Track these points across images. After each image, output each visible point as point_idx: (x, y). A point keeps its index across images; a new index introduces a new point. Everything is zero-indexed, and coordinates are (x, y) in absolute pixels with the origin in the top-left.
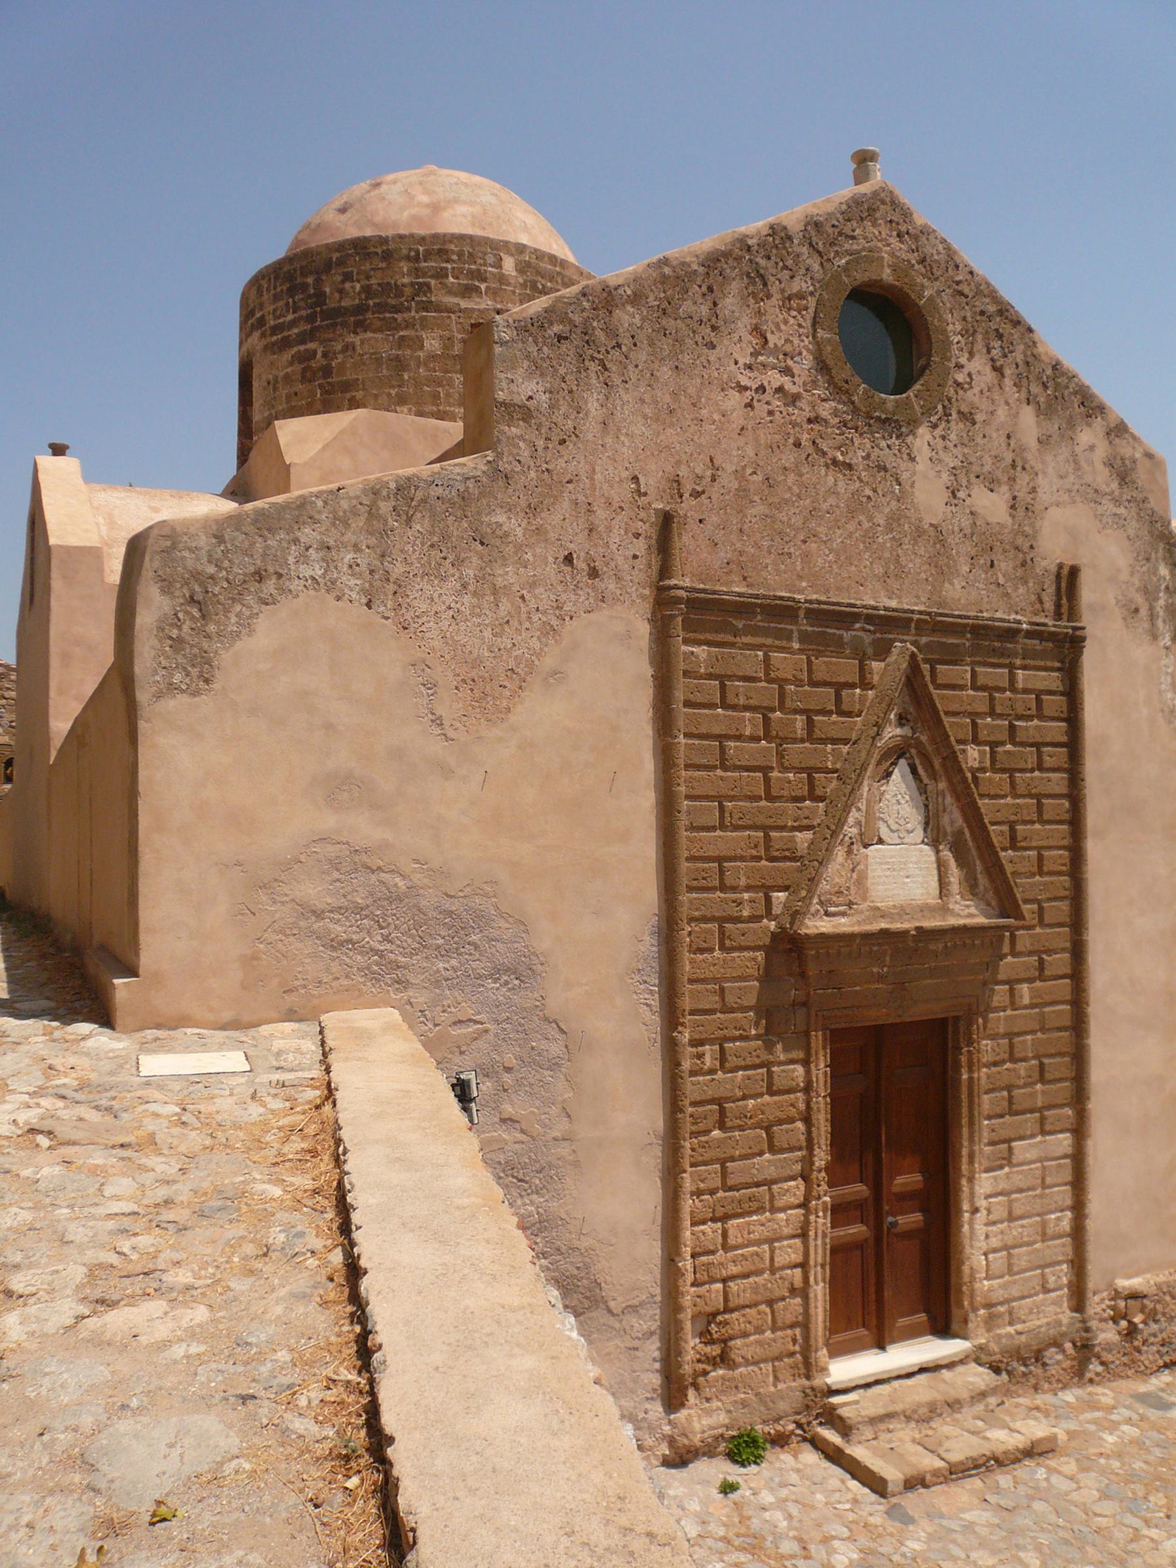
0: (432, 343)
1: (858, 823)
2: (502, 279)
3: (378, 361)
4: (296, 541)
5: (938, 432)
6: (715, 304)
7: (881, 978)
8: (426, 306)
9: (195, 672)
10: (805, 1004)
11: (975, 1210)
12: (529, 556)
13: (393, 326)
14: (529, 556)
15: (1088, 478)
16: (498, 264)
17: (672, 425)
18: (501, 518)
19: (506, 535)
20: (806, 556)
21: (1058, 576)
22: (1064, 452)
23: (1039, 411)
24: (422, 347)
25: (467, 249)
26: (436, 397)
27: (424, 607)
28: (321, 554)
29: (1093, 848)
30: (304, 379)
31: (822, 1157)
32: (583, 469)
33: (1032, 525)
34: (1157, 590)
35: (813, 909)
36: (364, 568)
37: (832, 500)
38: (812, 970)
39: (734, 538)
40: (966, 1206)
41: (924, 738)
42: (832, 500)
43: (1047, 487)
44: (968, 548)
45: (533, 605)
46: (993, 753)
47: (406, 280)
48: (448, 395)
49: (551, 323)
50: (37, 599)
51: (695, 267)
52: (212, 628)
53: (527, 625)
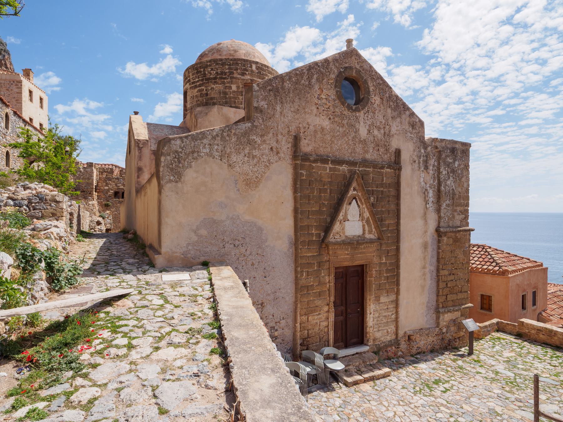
0: (234, 87)
1: (343, 215)
2: (252, 71)
4: (202, 143)
5: (365, 115)
6: (310, 81)
7: (348, 254)
9: (176, 176)
10: (328, 261)
11: (370, 314)
12: (262, 147)
14: (262, 147)
15: (404, 127)
16: (251, 67)
17: (298, 113)
18: (255, 138)
19: (256, 142)
20: (331, 147)
21: (395, 153)
22: (398, 120)
23: (392, 109)
24: (231, 89)
26: (235, 102)
27: (235, 160)
28: (209, 146)
29: (402, 221)
30: (201, 97)
32: (276, 125)
33: (389, 139)
34: (421, 156)
35: (331, 237)
36: (220, 150)
37: (338, 133)
38: (331, 253)
39: (313, 143)
40: (368, 312)
41: (360, 194)
42: (338, 133)
43: (394, 130)
44: (372, 145)
45: (262, 160)
46: (377, 198)
47: (227, 71)
48: (238, 102)
49: (268, 86)
50: (131, 153)
51: (304, 71)
52: (181, 165)
53: (261, 165)
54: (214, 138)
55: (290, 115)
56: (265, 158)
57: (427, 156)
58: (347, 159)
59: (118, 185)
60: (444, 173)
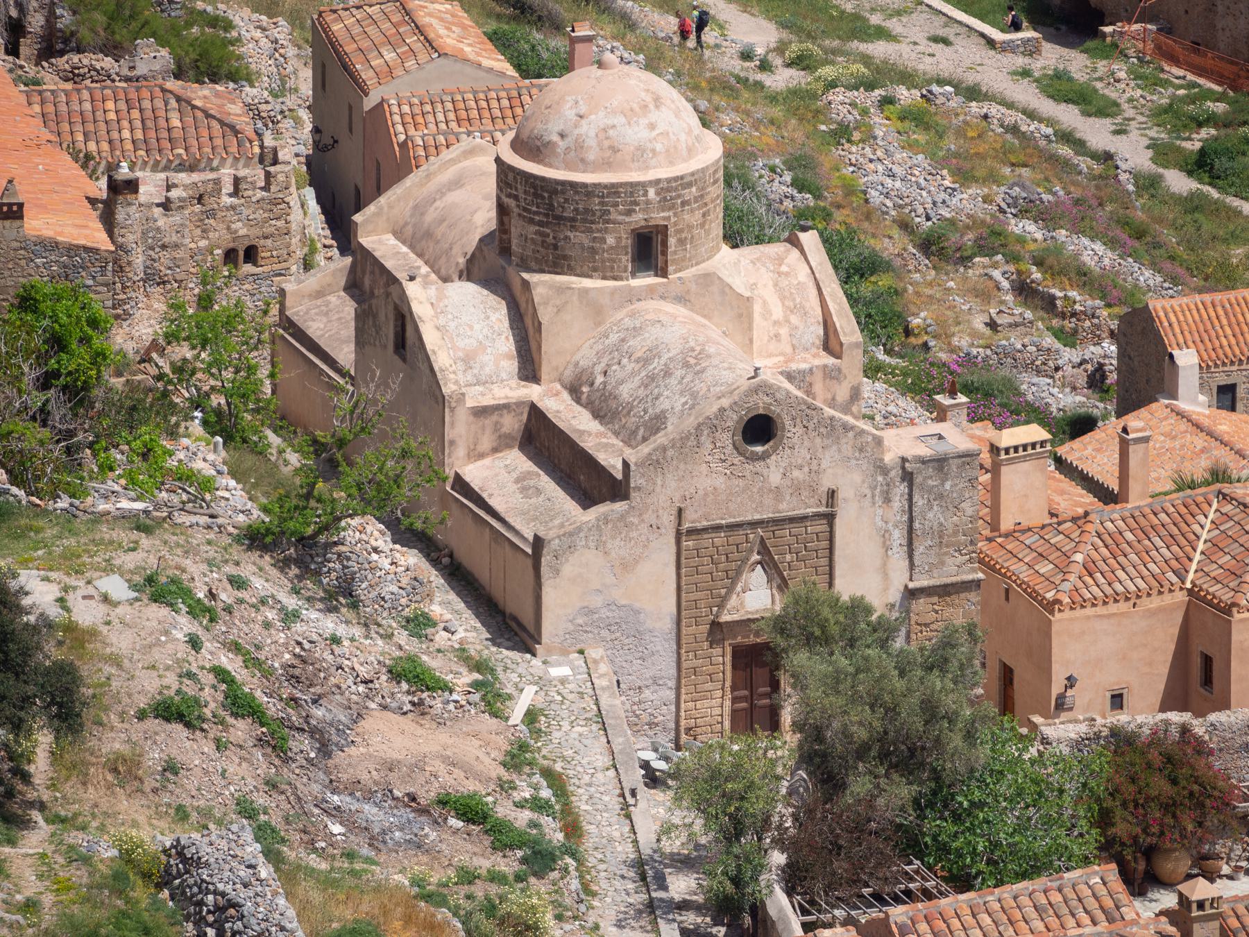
0: (611, 240)
2: (648, 202)
3: (583, 247)
8: (608, 222)
13: (590, 231)
16: (646, 194)
25: (630, 189)
26: (612, 268)
31: (728, 684)
54: (590, 530)
55: (673, 484)
56: (643, 538)
57: (888, 485)
58: (749, 518)
59: (233, 226)
60: (920, 503)
